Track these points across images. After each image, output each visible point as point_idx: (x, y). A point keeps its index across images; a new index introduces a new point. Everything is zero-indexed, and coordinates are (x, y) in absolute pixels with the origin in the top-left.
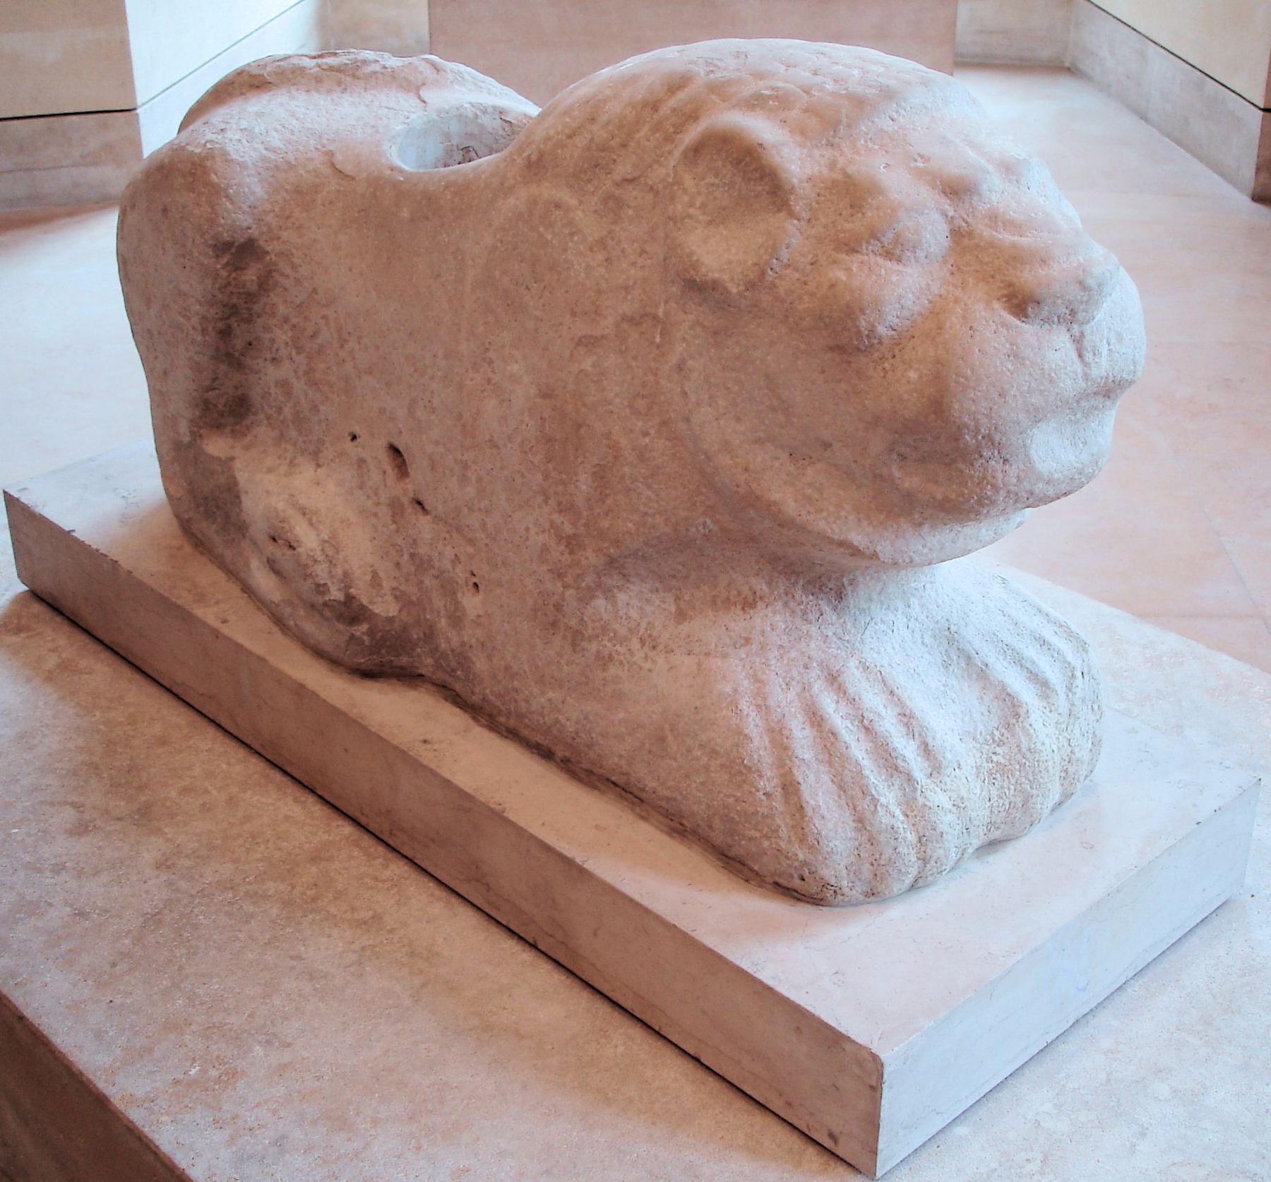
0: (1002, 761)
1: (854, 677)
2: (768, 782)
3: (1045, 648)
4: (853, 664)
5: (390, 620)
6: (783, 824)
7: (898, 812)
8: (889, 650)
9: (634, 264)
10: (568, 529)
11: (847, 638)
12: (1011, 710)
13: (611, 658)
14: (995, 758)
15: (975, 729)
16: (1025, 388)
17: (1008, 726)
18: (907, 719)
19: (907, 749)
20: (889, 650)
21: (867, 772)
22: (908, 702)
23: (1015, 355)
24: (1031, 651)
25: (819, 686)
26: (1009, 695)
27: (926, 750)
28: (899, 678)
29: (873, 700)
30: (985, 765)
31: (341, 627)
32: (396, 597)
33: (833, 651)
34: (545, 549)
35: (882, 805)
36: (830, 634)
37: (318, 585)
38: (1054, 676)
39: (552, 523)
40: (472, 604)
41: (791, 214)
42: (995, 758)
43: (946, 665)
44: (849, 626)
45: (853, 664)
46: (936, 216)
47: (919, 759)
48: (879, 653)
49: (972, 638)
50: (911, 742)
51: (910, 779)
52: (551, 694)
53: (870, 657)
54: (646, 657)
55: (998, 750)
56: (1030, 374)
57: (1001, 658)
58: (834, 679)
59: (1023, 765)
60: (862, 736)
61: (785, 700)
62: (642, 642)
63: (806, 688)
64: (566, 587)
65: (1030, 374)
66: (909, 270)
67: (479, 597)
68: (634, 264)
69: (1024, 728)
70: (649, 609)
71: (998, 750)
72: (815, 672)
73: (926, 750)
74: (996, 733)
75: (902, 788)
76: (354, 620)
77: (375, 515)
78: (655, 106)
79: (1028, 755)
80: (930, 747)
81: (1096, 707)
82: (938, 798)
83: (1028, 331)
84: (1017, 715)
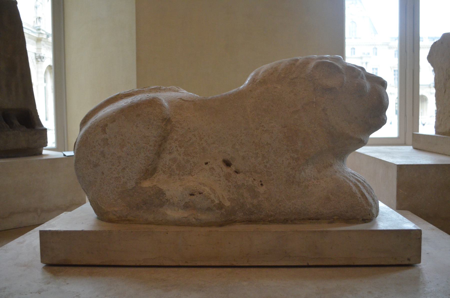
2: (359, 195)
5: (228, 207)
6: (364, 203)
9: (304, 93)
10: (296, 156)
13: (308, 185)
27: (367, 191)
31: (218, 211)
32: (229, 200)
34: (289, 163)
37: (212, 200)
39: (291, 156)
40: (261, 190)
41: (343, 73)
52: (293, 201)
54: (317, 182)
62: (314, 179)
64: (296, 171)
67: (264, 186)
68: (304, 93)
70: (312, 172)
76: (222, 208)
77: (220, 180)
78: (294, 64)
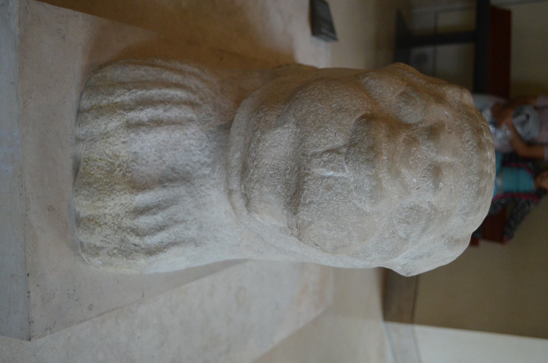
0: (116, 173)
1: (190, 114)
3: (158, 228)
4: (194, 116)
7: (119, 100)
8: (192, 142)
11: (207, 125)
12: (138, 186)
14: (118, 169)
15: (137, 164)
16: (320, 112)
17: (130, 182)
18: (158, 123)
19: (145, 114)
20: (192, 142)
21: (144, 91)
22: (166, 127)
23: (340, 110)
24: (159, 218)
25: (192, 97)
26: (145, 189)
27: (139, 125)
28: (177, 134)
29: (175, 113)
30: (117, 163)
33: (204, 114)
35: (126, 92)
36: (211, 118)
38: (144, 221)
42: (118, 169)
43: (173, 169)
44: (212, 129)
45: (194, 116)
46: (419, 119)
47: (138, 119)
48: (194, 134)
49: (180, 190)
50: (147, 120)
51: (131, 109)
53: (192, 129)
55: (122, 172)
56: (326, 115)
57: (164, 199)
58: (192, 104)
59: (107, 184)
60: (161, 99)
61: (193, 82)
63: (194, 92)
65: (326, 115)
66: (394, 98)
69: (125, 189)
71: (122, 172)
72: (198, 101)
73: (139, 125)
74: (130, 175)
75: (129, 105)
79: (111, 188)
80: (141, 127)
81: (115, 251)
82: (114, 123)
83: (350, 122)
84: (133, 188)
